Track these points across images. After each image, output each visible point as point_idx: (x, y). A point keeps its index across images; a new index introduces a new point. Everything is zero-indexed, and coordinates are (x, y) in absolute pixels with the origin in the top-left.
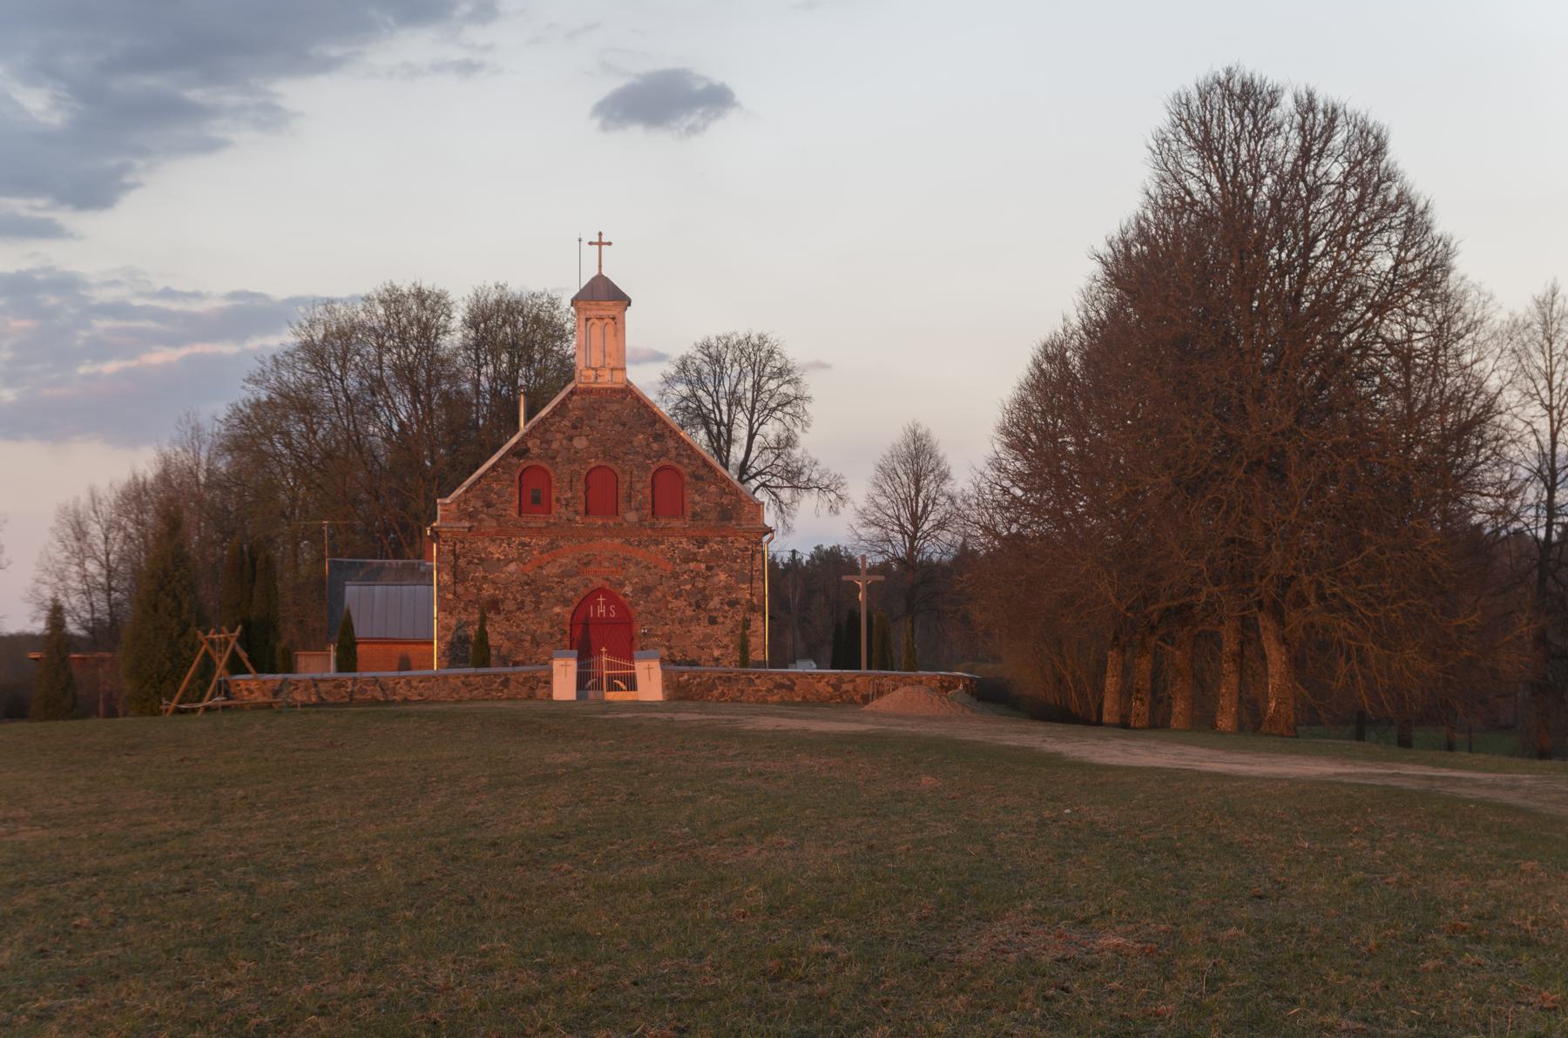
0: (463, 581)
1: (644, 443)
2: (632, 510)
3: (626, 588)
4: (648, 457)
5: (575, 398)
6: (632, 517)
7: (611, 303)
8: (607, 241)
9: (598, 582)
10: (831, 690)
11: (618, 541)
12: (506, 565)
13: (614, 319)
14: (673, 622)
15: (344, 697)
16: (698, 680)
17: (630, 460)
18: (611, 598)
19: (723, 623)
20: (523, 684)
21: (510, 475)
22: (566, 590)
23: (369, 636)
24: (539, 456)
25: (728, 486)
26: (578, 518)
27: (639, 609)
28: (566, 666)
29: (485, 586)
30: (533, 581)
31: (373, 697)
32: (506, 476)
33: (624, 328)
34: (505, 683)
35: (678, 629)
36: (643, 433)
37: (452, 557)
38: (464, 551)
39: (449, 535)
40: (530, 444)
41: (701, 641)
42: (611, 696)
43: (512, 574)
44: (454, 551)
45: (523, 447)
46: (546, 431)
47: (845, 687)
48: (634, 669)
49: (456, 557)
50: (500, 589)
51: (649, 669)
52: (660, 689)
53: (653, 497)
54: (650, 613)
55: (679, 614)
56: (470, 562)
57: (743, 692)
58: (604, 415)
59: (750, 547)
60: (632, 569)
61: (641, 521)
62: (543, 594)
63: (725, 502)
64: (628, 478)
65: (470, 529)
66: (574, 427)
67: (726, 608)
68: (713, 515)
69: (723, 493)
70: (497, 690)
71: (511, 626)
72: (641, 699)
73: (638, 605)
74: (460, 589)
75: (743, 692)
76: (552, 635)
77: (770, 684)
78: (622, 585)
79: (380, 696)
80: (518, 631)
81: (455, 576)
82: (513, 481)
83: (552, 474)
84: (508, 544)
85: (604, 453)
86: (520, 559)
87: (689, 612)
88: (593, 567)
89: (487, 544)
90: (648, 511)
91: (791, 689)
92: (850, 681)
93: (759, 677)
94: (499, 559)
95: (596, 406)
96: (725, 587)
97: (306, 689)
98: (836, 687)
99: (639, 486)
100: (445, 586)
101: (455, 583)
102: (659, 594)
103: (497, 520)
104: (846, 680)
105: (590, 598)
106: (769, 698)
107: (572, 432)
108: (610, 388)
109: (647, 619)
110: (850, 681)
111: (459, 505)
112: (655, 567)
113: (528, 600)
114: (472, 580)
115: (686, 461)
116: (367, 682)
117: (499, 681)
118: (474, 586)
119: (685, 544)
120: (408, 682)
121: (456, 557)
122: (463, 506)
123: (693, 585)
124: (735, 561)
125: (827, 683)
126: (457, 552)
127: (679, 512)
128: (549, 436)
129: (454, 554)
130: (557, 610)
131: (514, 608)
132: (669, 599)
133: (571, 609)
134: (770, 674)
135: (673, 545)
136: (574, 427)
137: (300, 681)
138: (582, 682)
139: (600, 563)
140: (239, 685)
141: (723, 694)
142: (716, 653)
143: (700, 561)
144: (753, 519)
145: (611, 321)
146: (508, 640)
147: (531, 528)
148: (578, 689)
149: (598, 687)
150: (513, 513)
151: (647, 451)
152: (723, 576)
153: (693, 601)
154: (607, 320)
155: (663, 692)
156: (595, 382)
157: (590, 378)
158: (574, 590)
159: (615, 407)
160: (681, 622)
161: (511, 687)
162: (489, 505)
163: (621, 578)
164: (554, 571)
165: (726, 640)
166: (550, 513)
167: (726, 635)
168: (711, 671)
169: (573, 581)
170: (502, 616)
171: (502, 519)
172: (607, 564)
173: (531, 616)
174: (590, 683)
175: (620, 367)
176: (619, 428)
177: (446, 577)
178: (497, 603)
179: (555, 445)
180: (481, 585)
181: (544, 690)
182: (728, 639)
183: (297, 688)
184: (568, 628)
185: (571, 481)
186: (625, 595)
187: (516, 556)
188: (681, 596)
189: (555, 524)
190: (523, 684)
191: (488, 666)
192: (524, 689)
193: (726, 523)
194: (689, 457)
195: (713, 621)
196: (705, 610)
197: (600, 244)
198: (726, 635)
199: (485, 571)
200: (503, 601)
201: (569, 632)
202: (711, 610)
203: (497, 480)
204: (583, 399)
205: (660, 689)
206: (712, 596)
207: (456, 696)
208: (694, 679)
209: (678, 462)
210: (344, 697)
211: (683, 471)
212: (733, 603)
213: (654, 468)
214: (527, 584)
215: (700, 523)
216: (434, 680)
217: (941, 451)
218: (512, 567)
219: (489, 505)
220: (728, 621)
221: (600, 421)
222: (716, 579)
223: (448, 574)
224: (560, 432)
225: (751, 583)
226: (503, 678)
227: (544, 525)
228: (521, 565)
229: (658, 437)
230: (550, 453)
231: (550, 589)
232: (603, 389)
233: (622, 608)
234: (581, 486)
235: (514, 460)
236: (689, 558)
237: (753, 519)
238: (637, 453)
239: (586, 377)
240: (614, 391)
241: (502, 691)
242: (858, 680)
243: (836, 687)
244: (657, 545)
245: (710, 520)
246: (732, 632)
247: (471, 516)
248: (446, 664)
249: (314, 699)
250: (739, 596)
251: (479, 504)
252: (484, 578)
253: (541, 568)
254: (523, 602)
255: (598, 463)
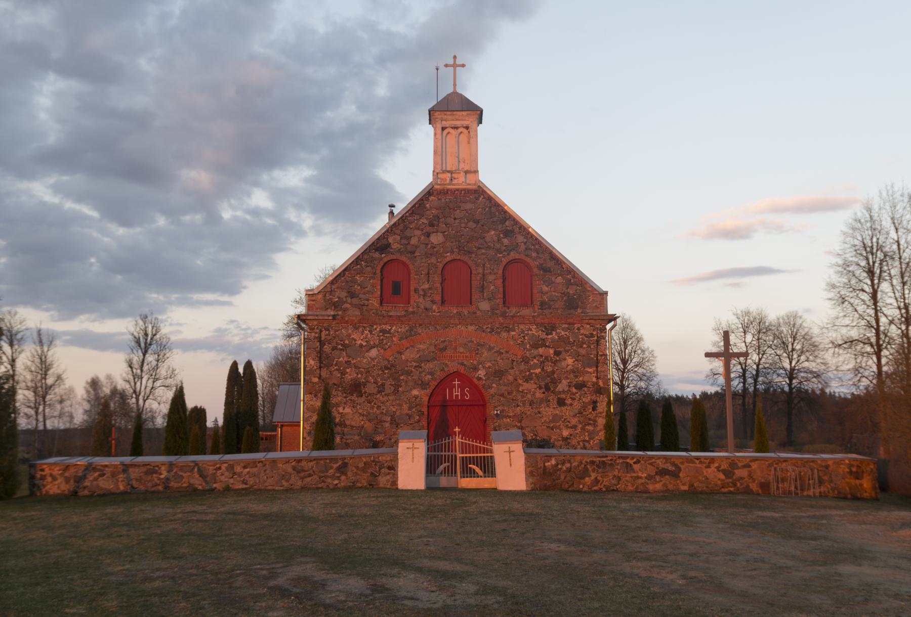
0: (328, 366)
1: (495, 238)
2: (485, 300)
3: (480, 372)
4: (499, 251)
5: (432, 198)
6: (485, 306)
7: (464, 113)
8: (461, 63)
9: (453, 367)
10: (722, 477)
11: (471, 328)
12: (368, 351)
13: (467, 128)
14: (524, 404)
15: (157, 485)
16: (568, 465)
17: (483, 254)
18: (467, 381)
19: (571, 405)
20: (364, 470)
21: (373, 268)
22: (423, 374)
23: (291, 421)
24: (399, 251)
25: (574, 277)
26: (434, 307)
27: (492, 391)
28: (413, 448)
29: (348, 370)
30: (393, 366)
31: (190, 485)
32: (369, 269)
33: (476, 135)
34: (343, 469)
35: (529, 410)
36: (494, 230)
37: (318, 344)
38: (329, 338)
39: (315, 323)
40: (391, 240)
41: (550, 422)
42: (466, 483)
43: (373, 359)
44: (320, 337)
45: (384, 242)
46: (406, 228)
47: (739, 473)
48: (491, 451)
49: (322, 344)
50: (362, 373)
51: (510, 452)
52: (522, 476)
53: (504, 287)
54: (502, 395)
55: (529, 396)
56: (334, 349)
57: (619, 479)
58: (458, 214)
59: (595, 333)
60: (486, 354)
61: (493, 309)
62: (402, 378)
63: (571, 292)
64: (480, 270)
65: (334, 317)
66: (431, 225)
67: (574, 390)
68: (560, 304)
69: (569, 284)
70: (333, 477)
71: (372, 408)
72: (502, 487)
73: (490, 387)
74: (324, 373)
75: (619, 479)
76: (410, 417)
77: (651, 470)
78: (476, 369)
79: (198, 483)
80: (378, 412)
81: (320, 361)
82: (375, 273)
83: (411, 267)
84: (370, 332)
85: (459, 248)
86: (380, 345)
87: (539, 394)
88: (449, 352)
89: (350, 331)
90: (499, 301)
91: (675, 475)
92: (744, 466)
93: (638, 462)
94: (361, 346)
95: (451, 206)
96: (573, 371)
97: (114, 475)
98: (728, 473)
99: (491, 278)
100: (311, 370)
101: (320, 367)
102: (511, 378)
103: (361, 310)
104: (740, 465)
105: (446, 381)
106: (651, 487)
107: (429, 229)
108: (464, 190)
109: (499, 400)
110: (744, 466)
111: (325, 296)
112: (507, 352)
113: (388, 383)
114: (336, 365)
115: (534, 254)
116: (183, 468)
117: (335, 466)
118: (338, 370)
119: (534, 331)
120: (231, 467)
121: (322, 344)
122: (328, 297)
123: (543, 369)
124: (581, 347)
125: (718, 468)
126: (323, 338)
127: (528, 302)
128: (408, 233)
129: (320, 341)
130: (415, 392)
131: (375, 391)
132: (520, 382)
133: (429, 391)
134: (651, 457)
135: (523, 332)
136: (431, 225)
137: (106, 466)
138: (432, 466)
139: (455, 348)
140: (43, 470)
141: (596, 481)
142: (565, 433)
143: (549, 347)
144: (597, 307)
145: (465, 131)
146: (369, 421)
147: (391, 316)
148: (427, 476)
149: (451, 471)
150: (375, 302)
151: (498, 246)
152: (570, 361)
153: (543, 384)
154: (460, 130)
155: (527, 481)
156: (449, 184)
157: (446, 180)
158: (432, 374)
159: (469, 206)
160: (531, 403)
161: (349, 474)
162: (352, 295)
163: (475, 362)
164: (412, 356)
165: (574, 421)
166: (409, 303)
167: (574, 416)
168: (583, 455)
169: (431, 365)
170: (364, 398)
171: (365, 308)
172: (462, 350)
173: (390, 398)
174: (442, 467)
175: (473, 170)
176: (472, 225)
177: (312, 362)
178: (360, 387)
179: (414, 241)
180: (345, 369)
181: (388, 477)
182: (576, 420)
183: (104, 475)
184: (425, 410)
185: (428, 274)
186: (479, 379)
187: (377, 342)
188: (531, 379)
189: (413, 312)
190: (364, 470)
191: (331, 448)
192: (365, 476)
193: (572, 311)
194: (537, 251)
195: (561, 403)
196: (554, 392)
197: (455, 66)
198: (574, 416)
199: (349, 357)
200: (365, 385)
201: (426, 413)
202: (560, 393)
203: (361, 273)
204: (439, 199)
205: (523, 476)
206: (560, 379)
207: (285, 484)
208: (563, 464)
209: (527, 256)
210: (157, 485)
211: (533, 264)
212: (580, 386)
213: (505, 261)
214: (387, 368)
215: (547, 311)
216: (261, 464)
217: (637, 327)
218: (374, 353)
219: (352, 295)
220: (576, 403)
221: (455, 219)
222: (563, 364)
223: (313, 359)
224: (418, 229)
225: (597, 367)
226: (340, 463)
227: (403, 313)
228: (382, 351)
229: (508, 233)
230: (409, 247)
231: (409, 373)
232: (458, 190)
233: (477, 391)
234: (437, 278)
235: (377, 255)
236: (538, 344)
237: (597, 307)
238: (489, 247)
239: (442, 179)
240: (467, 191)
241: (338, 478)
242: (754, 465)
243: (728, 473)
244: (508, 332)
245: (557, 309)
246: (580, 413)
247: (336, 306)
248: (311, 444)
249: (122, 488)
250: (586, 379)
251: (343, 294)
252: (348, 362)
253: (401, 353)
254: (383, 385)
255: (454, 257)
